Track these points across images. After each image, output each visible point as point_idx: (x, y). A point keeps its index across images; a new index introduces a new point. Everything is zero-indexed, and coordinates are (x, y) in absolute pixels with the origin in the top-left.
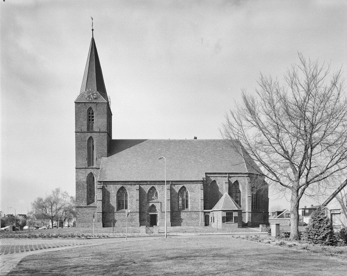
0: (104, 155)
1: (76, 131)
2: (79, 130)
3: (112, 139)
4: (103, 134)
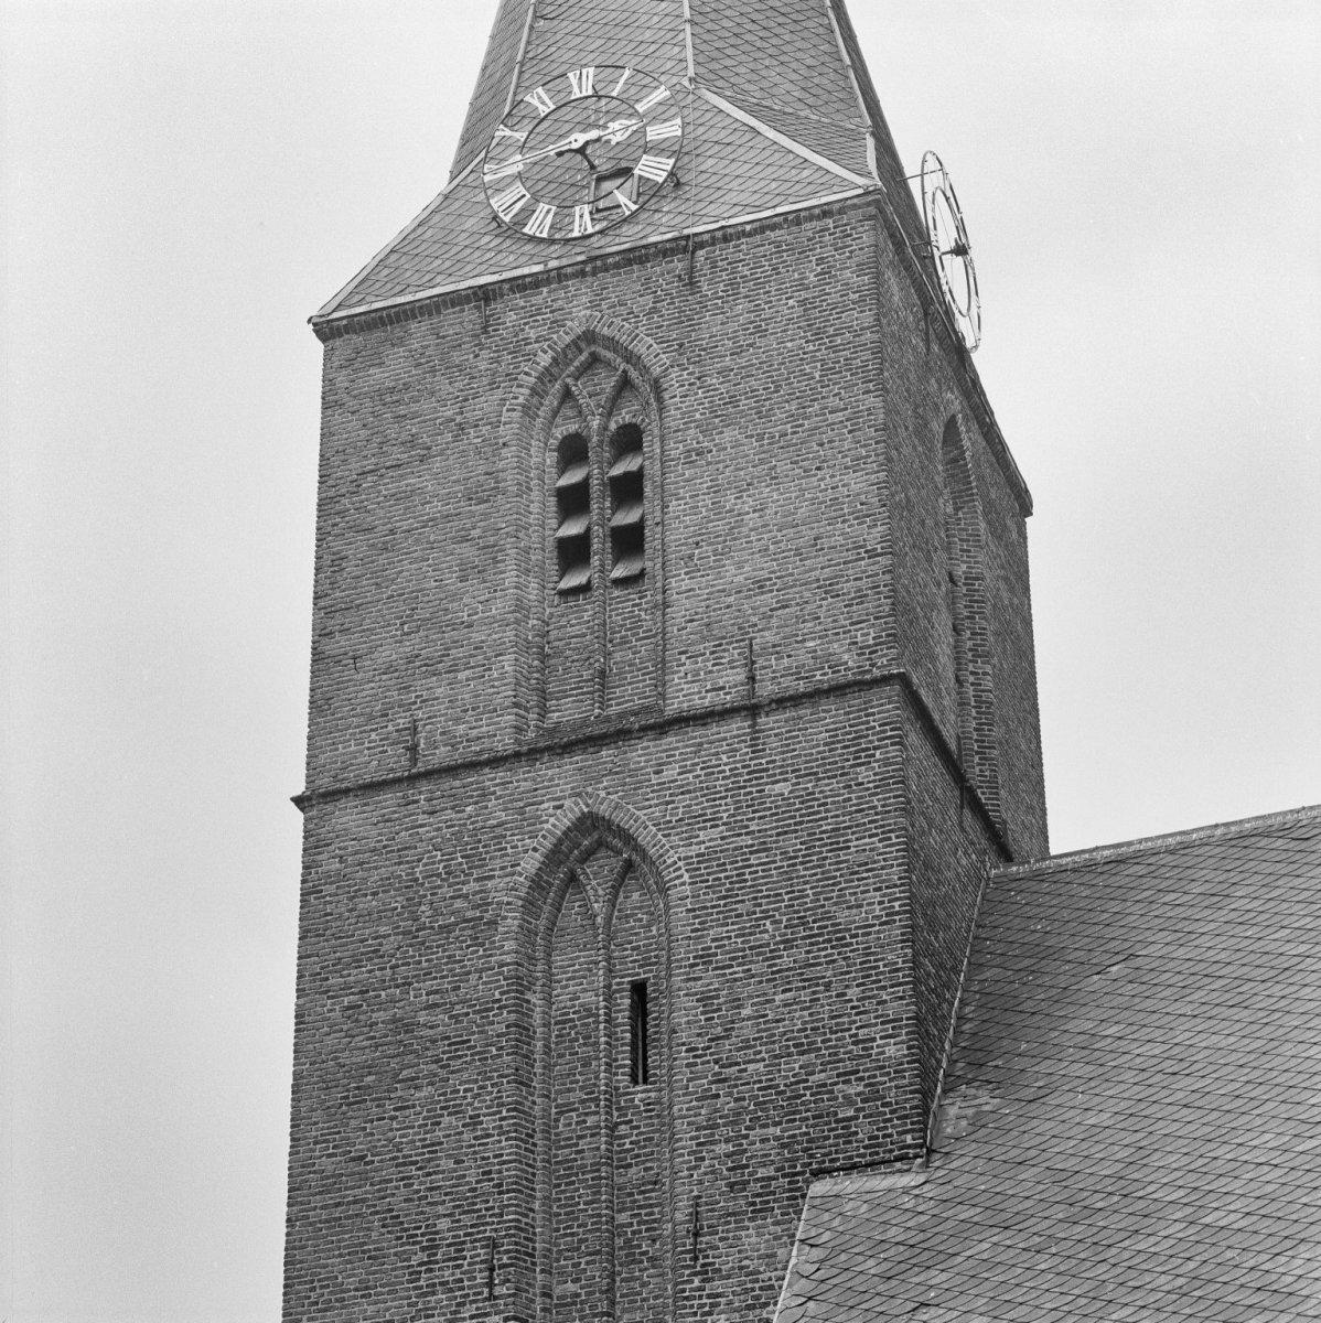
0: (863, 1130)
1: (325, 782)
2: (370, 756)
3: (1053, 851)
4: (823, 724)
